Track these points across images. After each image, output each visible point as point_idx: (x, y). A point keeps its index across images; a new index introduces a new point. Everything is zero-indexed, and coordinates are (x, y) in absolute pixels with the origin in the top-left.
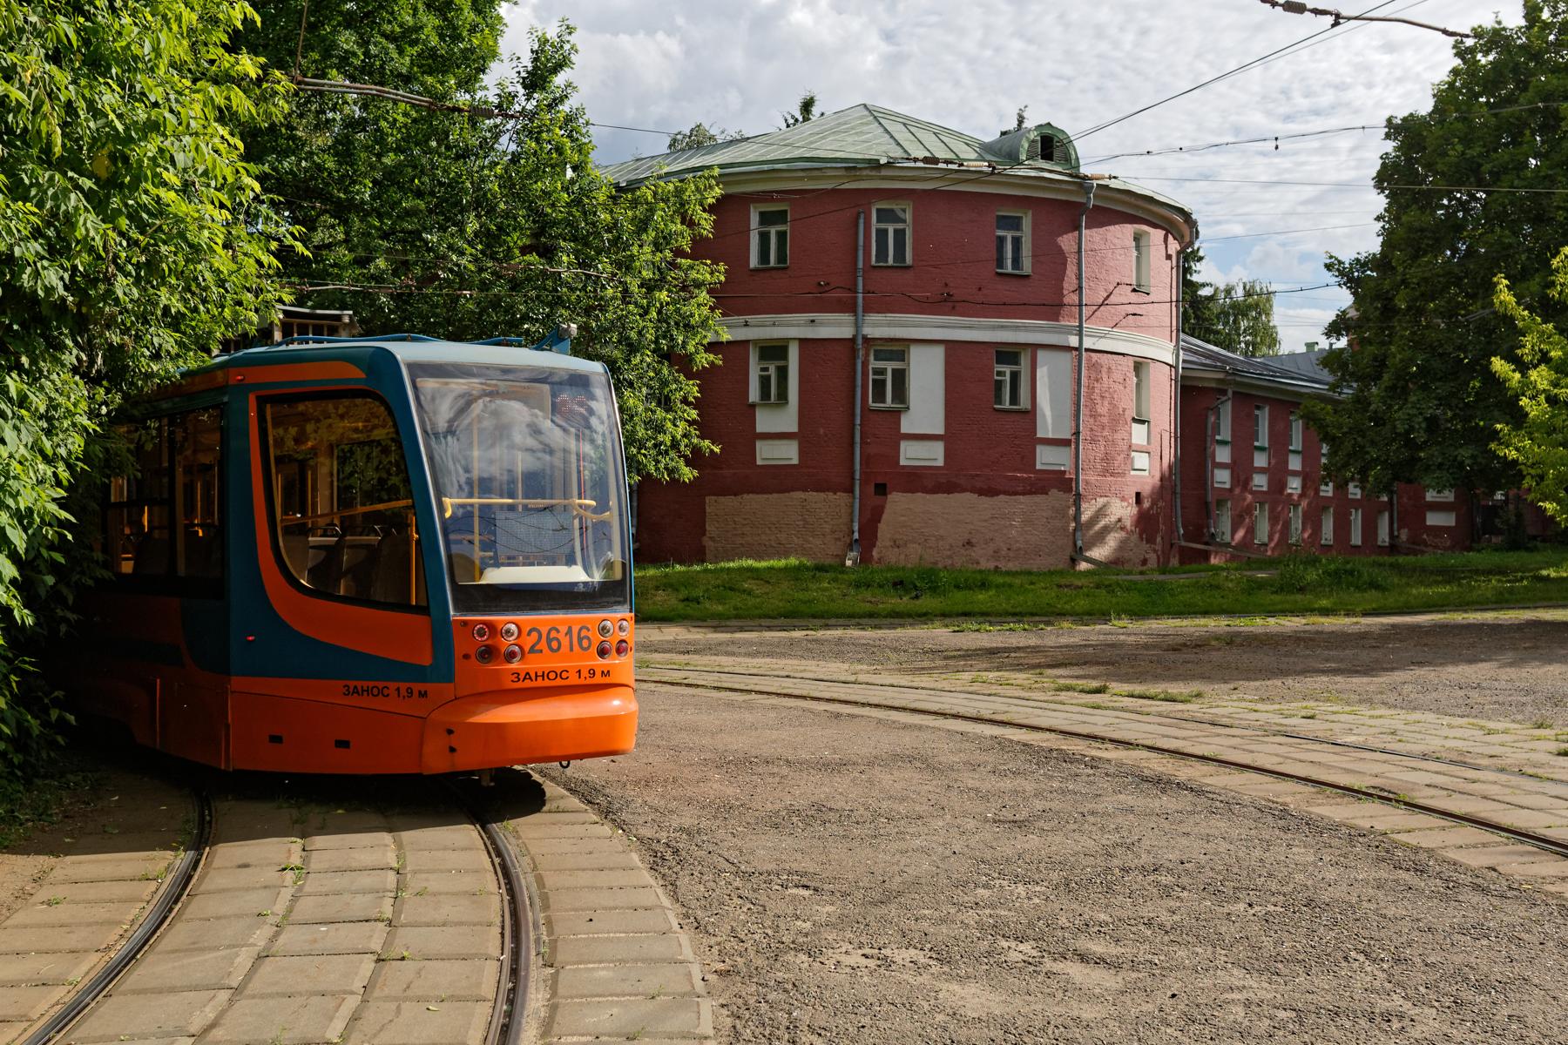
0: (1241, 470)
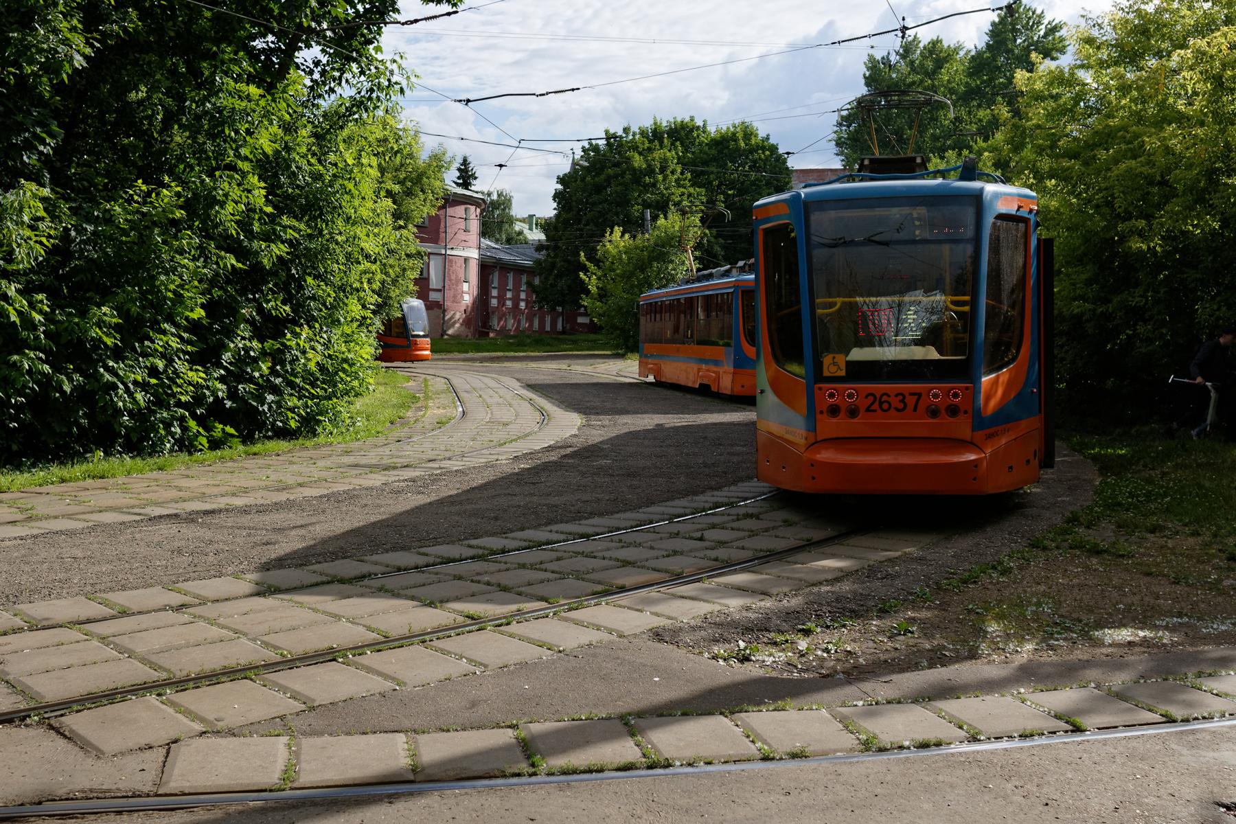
0: (501, 299)
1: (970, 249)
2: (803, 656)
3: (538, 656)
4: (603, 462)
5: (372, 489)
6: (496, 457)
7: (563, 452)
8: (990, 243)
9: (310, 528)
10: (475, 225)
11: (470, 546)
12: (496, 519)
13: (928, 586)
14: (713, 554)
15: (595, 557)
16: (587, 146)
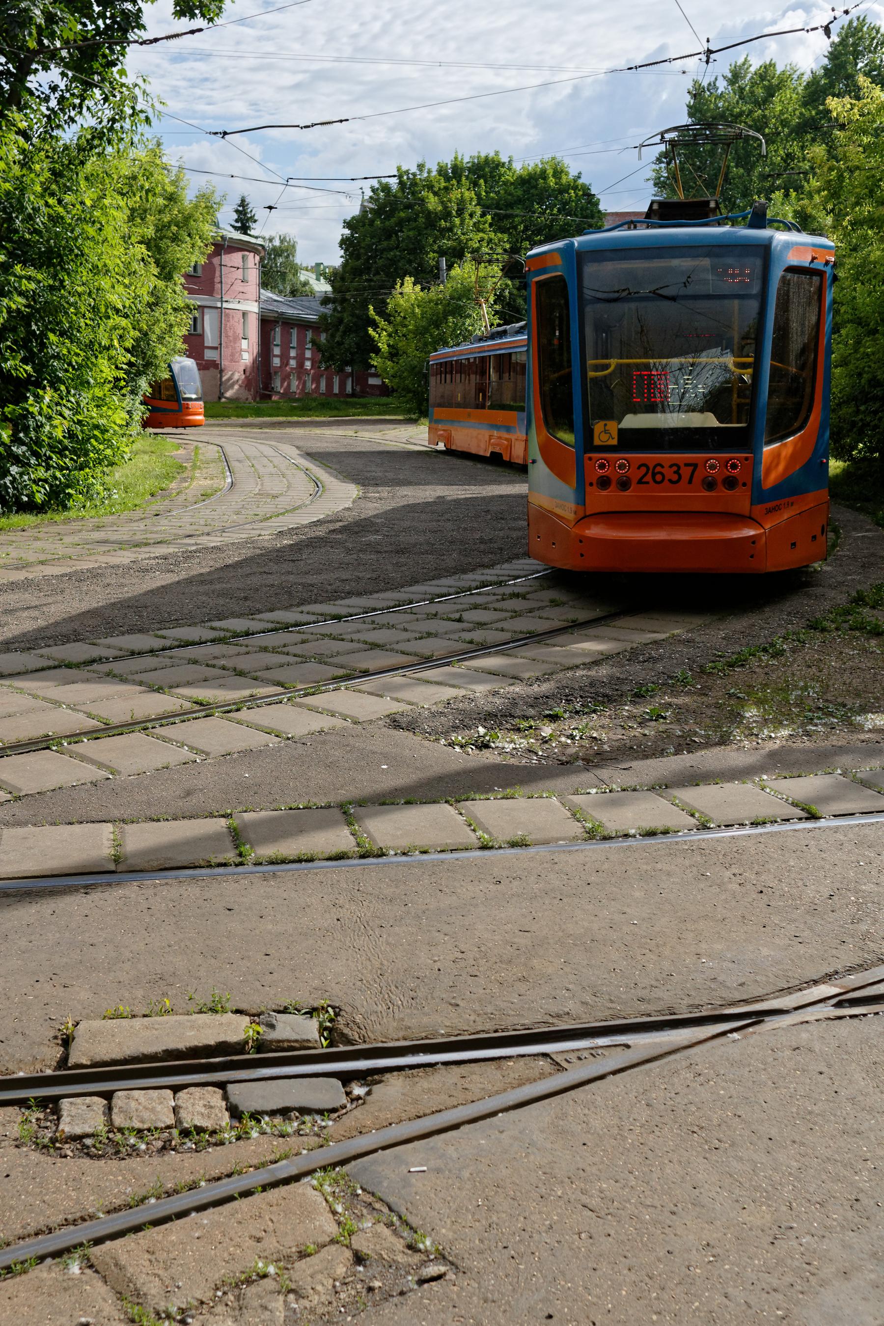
0: (285, 357)
1: (754, 305)
2: (546, 742)
3: (264, 743)
4: (372, 538)
5: (118, 567)
6: (258, 532)
7: (332, 527)
8: (778, 298)
9: (45, 609)
10: (254, 275)
11: (213, 629)
12: (246, 599)
13: (691, 670)
14: (468, 636)
15: (343, 640)
16: (377, 186)
